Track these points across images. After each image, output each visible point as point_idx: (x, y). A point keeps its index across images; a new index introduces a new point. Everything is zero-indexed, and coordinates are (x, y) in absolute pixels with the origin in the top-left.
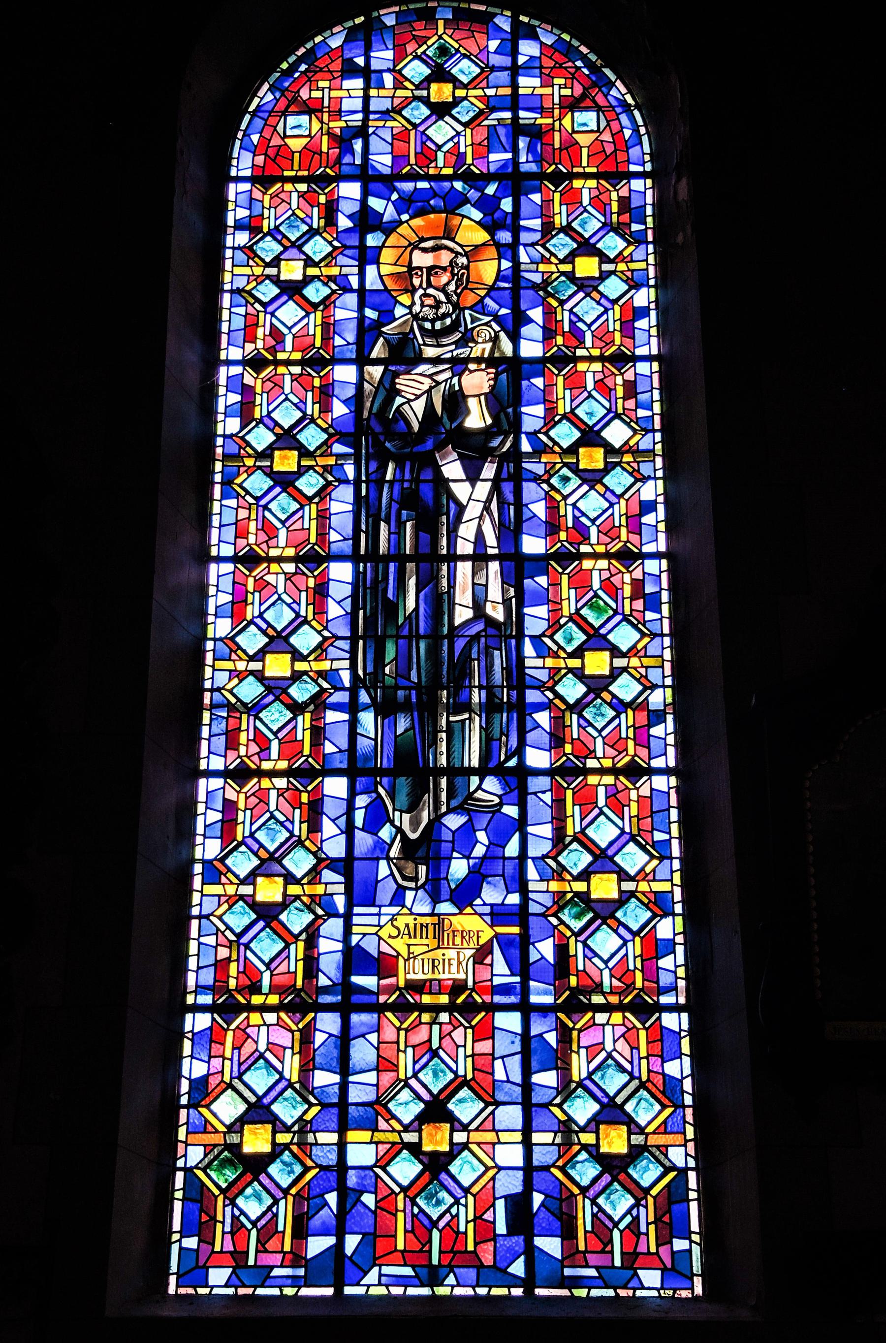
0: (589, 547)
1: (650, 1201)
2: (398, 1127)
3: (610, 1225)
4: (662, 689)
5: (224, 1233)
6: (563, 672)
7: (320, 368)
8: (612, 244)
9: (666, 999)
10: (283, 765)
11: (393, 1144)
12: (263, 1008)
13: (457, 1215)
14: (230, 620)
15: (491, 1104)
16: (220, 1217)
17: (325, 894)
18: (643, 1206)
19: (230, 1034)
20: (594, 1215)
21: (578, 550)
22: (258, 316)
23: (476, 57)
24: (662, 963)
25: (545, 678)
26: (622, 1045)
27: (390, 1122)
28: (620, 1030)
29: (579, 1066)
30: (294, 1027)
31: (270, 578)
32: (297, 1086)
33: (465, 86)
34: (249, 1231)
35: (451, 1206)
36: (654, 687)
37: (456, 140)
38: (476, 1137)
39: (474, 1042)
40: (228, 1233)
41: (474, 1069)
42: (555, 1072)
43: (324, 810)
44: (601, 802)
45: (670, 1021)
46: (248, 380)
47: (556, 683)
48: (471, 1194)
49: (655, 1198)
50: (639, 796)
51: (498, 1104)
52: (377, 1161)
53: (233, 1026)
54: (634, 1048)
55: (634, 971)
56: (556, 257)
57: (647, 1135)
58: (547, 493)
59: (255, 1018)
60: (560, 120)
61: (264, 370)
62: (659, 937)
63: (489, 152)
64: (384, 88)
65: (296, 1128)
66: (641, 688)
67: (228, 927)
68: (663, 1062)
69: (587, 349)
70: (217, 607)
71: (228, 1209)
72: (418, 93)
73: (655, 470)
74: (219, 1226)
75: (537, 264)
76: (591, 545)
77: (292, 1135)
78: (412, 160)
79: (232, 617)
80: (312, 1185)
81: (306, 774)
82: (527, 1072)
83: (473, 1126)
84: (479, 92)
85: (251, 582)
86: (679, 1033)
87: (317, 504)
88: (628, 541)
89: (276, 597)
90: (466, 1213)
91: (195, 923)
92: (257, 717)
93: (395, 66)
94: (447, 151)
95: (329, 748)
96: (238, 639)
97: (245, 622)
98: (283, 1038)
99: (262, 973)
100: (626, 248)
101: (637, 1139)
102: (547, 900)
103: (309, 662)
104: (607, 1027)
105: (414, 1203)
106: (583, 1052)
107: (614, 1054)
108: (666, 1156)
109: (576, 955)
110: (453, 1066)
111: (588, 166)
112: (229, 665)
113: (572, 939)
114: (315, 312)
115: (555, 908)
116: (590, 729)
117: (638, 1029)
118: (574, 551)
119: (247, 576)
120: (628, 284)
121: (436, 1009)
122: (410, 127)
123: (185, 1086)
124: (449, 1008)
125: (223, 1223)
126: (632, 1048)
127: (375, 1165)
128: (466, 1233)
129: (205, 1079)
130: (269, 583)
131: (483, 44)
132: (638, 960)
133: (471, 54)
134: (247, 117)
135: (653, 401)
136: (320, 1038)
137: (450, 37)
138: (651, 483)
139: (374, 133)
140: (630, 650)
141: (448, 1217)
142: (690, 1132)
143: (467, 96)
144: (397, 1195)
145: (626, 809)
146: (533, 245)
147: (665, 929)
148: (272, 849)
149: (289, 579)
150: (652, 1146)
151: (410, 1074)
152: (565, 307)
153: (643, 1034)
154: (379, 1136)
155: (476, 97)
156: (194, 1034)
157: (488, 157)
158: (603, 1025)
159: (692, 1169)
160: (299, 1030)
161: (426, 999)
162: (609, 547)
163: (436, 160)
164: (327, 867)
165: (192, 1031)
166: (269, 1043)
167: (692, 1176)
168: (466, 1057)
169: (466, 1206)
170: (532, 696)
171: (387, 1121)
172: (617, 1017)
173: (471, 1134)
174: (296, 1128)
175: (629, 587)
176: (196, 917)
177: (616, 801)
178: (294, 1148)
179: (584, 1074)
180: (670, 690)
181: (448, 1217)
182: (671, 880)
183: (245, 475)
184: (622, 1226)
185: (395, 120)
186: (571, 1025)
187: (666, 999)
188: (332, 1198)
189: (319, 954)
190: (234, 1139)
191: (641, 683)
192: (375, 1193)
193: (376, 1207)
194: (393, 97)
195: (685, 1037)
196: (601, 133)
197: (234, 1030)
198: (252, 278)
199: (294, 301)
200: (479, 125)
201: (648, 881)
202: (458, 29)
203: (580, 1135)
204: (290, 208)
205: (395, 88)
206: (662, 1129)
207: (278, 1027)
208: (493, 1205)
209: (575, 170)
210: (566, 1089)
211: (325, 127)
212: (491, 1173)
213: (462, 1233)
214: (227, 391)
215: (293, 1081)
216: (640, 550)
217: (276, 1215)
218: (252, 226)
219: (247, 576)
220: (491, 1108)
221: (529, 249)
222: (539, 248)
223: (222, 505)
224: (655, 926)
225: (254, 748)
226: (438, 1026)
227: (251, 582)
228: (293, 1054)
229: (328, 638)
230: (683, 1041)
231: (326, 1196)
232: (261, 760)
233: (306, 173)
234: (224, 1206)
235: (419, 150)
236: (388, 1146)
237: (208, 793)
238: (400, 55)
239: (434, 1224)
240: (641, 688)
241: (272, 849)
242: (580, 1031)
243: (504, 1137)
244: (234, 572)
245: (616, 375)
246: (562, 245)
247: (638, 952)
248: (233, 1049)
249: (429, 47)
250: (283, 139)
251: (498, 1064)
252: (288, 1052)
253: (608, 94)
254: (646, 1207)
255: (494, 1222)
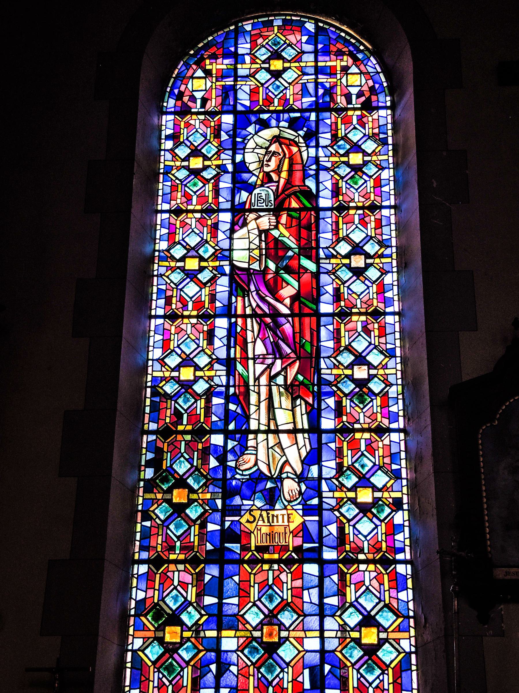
0: (363, 555)
1: (390, 670)
2: (250, 628)
3: (367, 685)
4: (388, 170)
5: (154, 687)
6: (345, 500)
7: (207, 320)
8: (370, 146)
9: (400, 556)
10: (195, 313)
11: (247, 637)
12: (176, 562)
13: (283, 678)
14: (167, 242)
15: (302, 616)
16: (151, 678)
17: (211, 499)
18: (386, 674)
19: (158, 576)
20: (358, 679)
21: (357, 557)
22: (178, 186)
23: (295, 45)
24: (397, 537)
25: (330, 269)
26: (375, 583)
27: (246, 625)
28: (374, 574)
29: (351, 594)
30: (193, 572)
31: (192, 122)
32: (195, 604)
33: (289, 61)
34: (168, 687)
35: (280, 673)
36: (391, 385)
37: (284, 92)
38: (293, 634)
39: (292, 581)
40: (156, 687)
41: (292, 596)
42: (337, 597)
43: (216, 334)
44: (363, 448)
45: (401, 569)
46: (160, 444)
47: (339, 382)
48: (291, 666)
49: (393, 669)
50: (383, 445)
51: (305, 616)
52: (238, 647)
53: (159, 572)
54: (381, 584)
55: (381, 542)
56: (342, 365)
57: (388, 632)
58: (332, 176)
59: (172, 567)
60: (341, 79)
61: (176, 321)
62: (395, 523)
63: (302, 98)
64: (245, 63)
65: (194, 628)
66: (380, 274)
67: (172, 282)
68: (398, 592)
69: (356, 202)
70: (160, 236)
71: (156, 674)
72: (263, 66)
73: (392, 267)
74: (151, 683)
75: (329, 157)
76: (361, 424)
77: (191, 632)
78: (261, 103)
79: (168, 241)
80: (202, 660)
81: (209, 211)
82: (321, 596)
83: (291, 628)
84: (297, 64)
85: (182, 124)
86: (406, 576)
87: (209, 287)
88: (375, 200)
89: (195, 130)
90: (287, 677)
91: (155, 279)
92: (176, 402)
93: (251, 52)
94: (280, 98)
95: (214, 418)
96: (166, 360)
97: (170, 351)
98: (188, 578)
99: (188, 302)
100: (379, 250)
101: (383, 635)
102: (333, 502)
103: (208, 262)
104: (366, 572)
105: (259, 672)
106: (353, 586)
107: (370, 587)
108: (399, 644)
109: (349, 534)
110: (281, 594)
111: (356, 104)
112: (167, 264)
113: (342, 286)
114: (205, 288)
115: (338, 507)
116: (360, 536)
117: (383, 574)
118: (351, 427)
119: (181, 121)
120: (380, 271)
121: (271, 562)
122: (260, 85)
123: (133, 604)
124: (278, 562)
125: (153, 681)
126: (380, 584)
127: (237, 650)
128: (287, 689)
129: (144, 600)
130: (187, 224)
131: (299, 38)
132: (384, 536)
133: (292, 44)
134: (172, 80)
135: (392, 253)
136: (207, 578)
137: (281, 34)
138: (390, 275)
139: (240, 88)
140: (372, 153)
141: (277, 679)
142: (412, 632)
143: (288, 637)
144: (249, 667)
145: (377, 452)
146: (328, 357)
147: (399, 518)
148: (188, 353)
149: (194, 326)
150: (390, 639)
151: (256, 598)
152: (345, 285)
153: (386, 577)
154: (238, 634)
155: (295, 67)
156: (138, 576)
157: (301, 100)
158: (364, 571)
159: (413, 653)
160: (196, 573)
161: (266, 556)
162: (371, 425)
163: (274, 103)
164: (216, 362)
165: (137, 574)
166: (179, 581)
167: (413, 656)
168: (288, 590)
169: (288, 673)
170: (326, 389)
171: (244, 625)
172: (372, 567)
173: (291, 632)
174: (194, 628)
175: (374, 223)
176: (156, 276)
177: (371, 449)
178: (193, 640)
179: (353, 599)
180: (392, 170)
181: (277, 679)
182: (402, 491)
183: (176, 170)
184: (374, 685)
185: (252, 81)
186: (346, 571)
187: (400, 556)
188: (213, 667)
189: (212, 405)
190: (160, 634)
191: (384, 383)
192: (237, 665)
193: (238, 673)
194: (250, 69)
195: (409, 578)
196: (362, 87)
197: (160, 574)
198: (155, 501)
199: (194, 282)
200: (297, 83)
201: (389, 492)
202: (285, 29)
203: (350, 633)
204: (191, 228)
205: (251, 63)
206: (397, 629)
207: (184, 573)
208: (303, 673)
209: (349, 106)
210: (343, 607)
211: (214, 84)
212: (302, 654)
213: (285, 688)
214: (161, 227)
215: (192, 601)
216: (381, 204)
217: (182, 677)
218: (175, 137)
219: (181, 121)
220: (301, 618)
221: (325, 149)
222: (332, 359)
223: (163, 185)
224: (383, 279)
225: (179, 305)
226: (272, 571)
227: (182, 124)
228: (193, 587)
229: (218, 250)
230: (408, 581)
231: (210, 666)
232: (183, 311)
233: (203, 110)
234: (154, 672)
235: (264, 97)
236: (244, 639)
237: (156, 326)
238: (254, 44)
239: (270, 683)
240: (380, 274)
241: (188, 353)
242: (351, 574)
243: (309, 634)
244: (174, 120)
245: (374, 323)
246: (347, 358)
247: (384, 531)
248: (160, 584)
249: (270, 40)
250: (191, 92)
251: (306, 593)
252: (190, 586)
253: (366, 65)
254: (388, 674)
255: (303, 683)
